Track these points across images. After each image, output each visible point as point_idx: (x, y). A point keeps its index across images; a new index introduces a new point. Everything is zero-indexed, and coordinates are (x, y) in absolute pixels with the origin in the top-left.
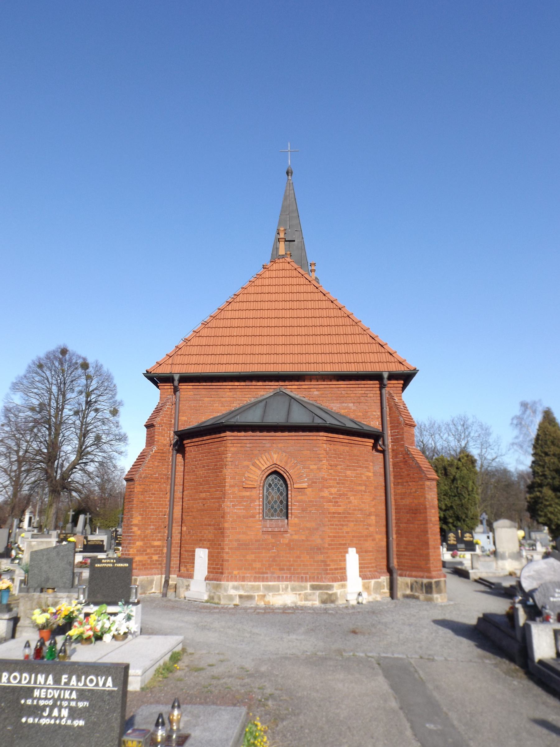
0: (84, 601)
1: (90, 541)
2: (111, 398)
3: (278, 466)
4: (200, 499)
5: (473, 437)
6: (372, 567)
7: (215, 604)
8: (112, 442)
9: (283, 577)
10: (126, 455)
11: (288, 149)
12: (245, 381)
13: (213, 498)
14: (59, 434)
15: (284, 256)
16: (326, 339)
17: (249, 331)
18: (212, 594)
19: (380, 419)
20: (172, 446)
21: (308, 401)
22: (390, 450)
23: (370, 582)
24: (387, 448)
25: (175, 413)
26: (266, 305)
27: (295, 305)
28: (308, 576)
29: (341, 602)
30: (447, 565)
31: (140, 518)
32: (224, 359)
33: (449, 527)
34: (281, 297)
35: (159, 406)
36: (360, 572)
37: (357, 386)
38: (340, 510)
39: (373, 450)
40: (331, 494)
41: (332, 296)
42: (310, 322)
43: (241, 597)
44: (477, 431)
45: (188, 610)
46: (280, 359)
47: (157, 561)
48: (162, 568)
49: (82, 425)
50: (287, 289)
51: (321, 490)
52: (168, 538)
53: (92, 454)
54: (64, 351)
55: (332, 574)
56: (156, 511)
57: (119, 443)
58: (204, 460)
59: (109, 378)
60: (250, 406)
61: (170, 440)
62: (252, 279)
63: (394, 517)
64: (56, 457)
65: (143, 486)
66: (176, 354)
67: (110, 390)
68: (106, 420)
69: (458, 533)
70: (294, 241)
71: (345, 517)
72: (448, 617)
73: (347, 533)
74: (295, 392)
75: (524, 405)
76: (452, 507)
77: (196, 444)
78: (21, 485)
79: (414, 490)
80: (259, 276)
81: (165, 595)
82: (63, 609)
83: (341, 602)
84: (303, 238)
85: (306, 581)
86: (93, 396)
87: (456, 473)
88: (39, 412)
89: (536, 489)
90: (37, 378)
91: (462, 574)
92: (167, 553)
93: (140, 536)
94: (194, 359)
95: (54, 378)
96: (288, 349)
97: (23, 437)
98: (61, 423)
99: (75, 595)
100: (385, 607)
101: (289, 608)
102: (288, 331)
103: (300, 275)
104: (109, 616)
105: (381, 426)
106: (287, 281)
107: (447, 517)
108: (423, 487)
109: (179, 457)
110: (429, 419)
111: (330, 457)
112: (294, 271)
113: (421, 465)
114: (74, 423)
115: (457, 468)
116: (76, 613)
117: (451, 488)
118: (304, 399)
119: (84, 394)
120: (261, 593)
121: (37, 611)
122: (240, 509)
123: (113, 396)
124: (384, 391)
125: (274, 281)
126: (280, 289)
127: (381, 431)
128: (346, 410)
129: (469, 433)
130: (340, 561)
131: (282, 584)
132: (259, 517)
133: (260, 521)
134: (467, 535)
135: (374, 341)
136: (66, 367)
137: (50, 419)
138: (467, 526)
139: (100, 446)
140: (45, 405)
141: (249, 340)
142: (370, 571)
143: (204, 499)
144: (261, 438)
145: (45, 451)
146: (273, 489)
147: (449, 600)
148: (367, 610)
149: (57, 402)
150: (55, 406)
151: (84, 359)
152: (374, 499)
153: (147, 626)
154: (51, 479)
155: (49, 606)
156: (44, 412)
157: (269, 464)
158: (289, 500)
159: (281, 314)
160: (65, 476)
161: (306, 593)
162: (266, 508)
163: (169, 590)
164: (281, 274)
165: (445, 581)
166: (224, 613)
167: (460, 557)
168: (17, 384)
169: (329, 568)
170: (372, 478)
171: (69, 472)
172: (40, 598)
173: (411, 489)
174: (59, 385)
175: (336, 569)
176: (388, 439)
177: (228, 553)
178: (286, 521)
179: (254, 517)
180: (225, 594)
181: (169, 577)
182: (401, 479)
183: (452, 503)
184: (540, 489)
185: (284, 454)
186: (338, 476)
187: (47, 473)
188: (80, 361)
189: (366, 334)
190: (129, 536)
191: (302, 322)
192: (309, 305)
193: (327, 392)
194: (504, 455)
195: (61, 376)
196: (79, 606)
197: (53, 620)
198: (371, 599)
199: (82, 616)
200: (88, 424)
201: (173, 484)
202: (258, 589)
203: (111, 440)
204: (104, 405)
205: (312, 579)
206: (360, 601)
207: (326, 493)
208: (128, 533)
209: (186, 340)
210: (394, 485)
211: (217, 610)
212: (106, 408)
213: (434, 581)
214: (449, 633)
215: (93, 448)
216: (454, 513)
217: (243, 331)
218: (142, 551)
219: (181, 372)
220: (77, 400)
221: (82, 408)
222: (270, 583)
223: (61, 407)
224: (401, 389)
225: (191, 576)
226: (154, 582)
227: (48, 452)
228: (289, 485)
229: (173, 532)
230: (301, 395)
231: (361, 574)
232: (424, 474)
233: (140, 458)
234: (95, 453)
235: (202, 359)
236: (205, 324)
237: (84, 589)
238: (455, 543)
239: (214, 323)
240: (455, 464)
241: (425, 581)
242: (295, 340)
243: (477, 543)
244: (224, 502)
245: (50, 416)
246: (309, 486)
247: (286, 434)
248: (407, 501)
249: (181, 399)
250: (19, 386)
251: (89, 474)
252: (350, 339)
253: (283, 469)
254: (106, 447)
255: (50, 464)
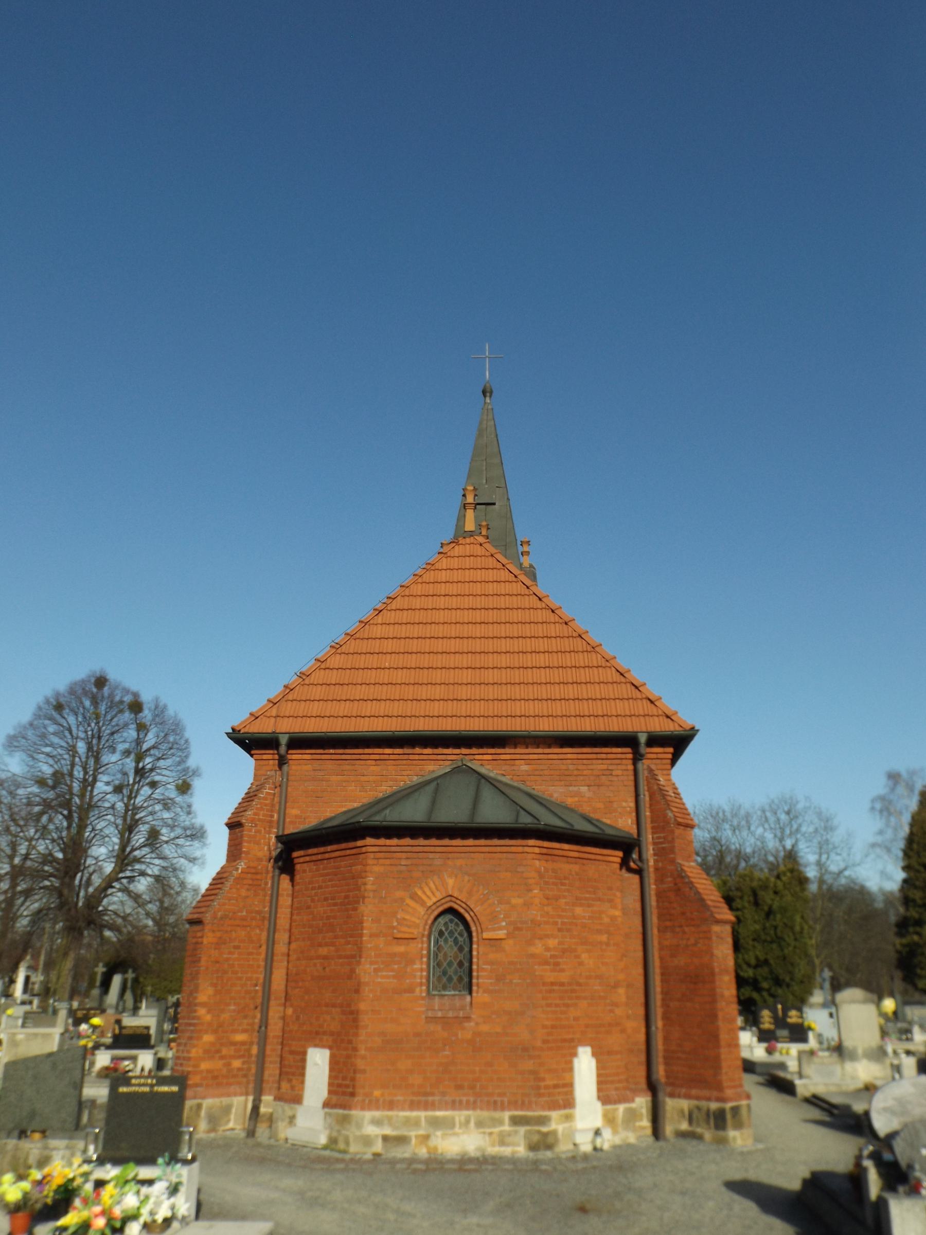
0: (95, 1157)
1: (125, 1028)
2: (179, 763)
3: (454, 899)
4: (318, 957)
5: (805, 833)
6: (620, 1081)
7: (340, 1152)
8: (180, 841)
9: (461, 1102)
10: (203, 863)
11: (485, 354)
12: (401, 747)
13: (340, 957)
14: (86, 826)
15: (473, 534)
16: (542, 676)
17: (412, 661)
18: (335, 1134)
19: (634, 814)
20: (272, 861)
21: (509, 782)
22: (651, 870)
23: (617, 1109)
24: (645, 866)
25: (280, 803)
26: (441, 616)
27: (491, 616)
28: (506, 1100)
29: (563, 1148)
30: (758, 1069)
31: (210, 991)
32: (368, 708)
33: (762, 996)
34: (468, 602)
35: (252, 790)
36: (599, 1090)
37: (594, 756)
38: (564, 977)
39: (621, 869)
40: (548, 949)
41: (554, 602)
42: (517, 645)
43: (385, 1138)
44: (812, 823)
45: (289, 1165)
46: (463, 708)
47: (239, 1069)
48: (248, 1083)
49: (127, 810)
50: (478, 589)
51: (530, 943)
52: (260, 1027)
53: (143, 862)
54: (101, 682)
55: (550, 1095)
56: (240, 979)
57: (191, 843)
58: (327, 887)
59: (177, 728)
60: (409, 790)
61: (269, 849)
62: (419, 572)
63: (658, 989)
64: (79, 865)
65: (218, 934)
66: (284, 699)
67: (178, 749)
68: (169, 801)
69: (776, 1009)
70: (494, 504)
71: (573, 991)
72: (754, 1175)
73: (576, 1019)
74: (488, 767)
75: (894, 777)
76: (766, 962)
77: (314, 858)
78: (15, 919)
79: (692, 941)
80: (430, 567)
81: (251, 1133)
82: (55, 1174)
83: (563, 1148)
84: (508, 499)
85: (503, 1109)
86: (148, 760)
87: (773, 900)
88: (53, 788)
89: (911, 929)
90: (52, 728)
91: (783, 1086)
92: (257, 1056)
93: (210, 1024)
94: (315, 708)
95: (81, 728)
96: (478, 692)
97: (22, 831)
98: (91, 806)
99: (81, 1144)
100: (642, 1157)
101: (471, 1160)
102: (478, 661)
103: (499, 566)
104: (139, 1186)
105: (635, 826)
106: (479, 575)
107: (759, 978)
108: (707, 936)
109: (285, 880)
110: (729, 801)
111: (546, 883)
112: (490, 558)
113: (705, 897)
114: (113, 807)
115: (776, 893)
116: (79, 1181)
117: (764, 929)
118: (503, 779)
119: (132, 756)
120: (422, 1132)
121: (8, 1177)
122: (388, 977)
123: (182, 761)
124: (640, 765)
125: (457, 576)
126: (466, 588)
127: (635, 836)
128: (576, 799)
129: (800, 826)
130: (564, 1070)
131: (459, 1116)
132: (421, 991)
133: (423, 998)
134: (793, 1013)
135: (623, 680)
136: (103, 708)
137: (71, 799)
138: (793, 994)
139: (157, 848)
140: (63, 775)
141: (410, 676)
142: (617, 1089)
143: (325, 958)
144: (426, 849)
145: (60, 855)
146: (446, 941)
147: (757, 1140)
148: (609, 1163)
149: (85, 769)
150: (81, 776)
151: (136, 695)
152: (624, 955)
153: (212, 1199)
154: (67, 907)
155: (30, 1167)
156: (61, 788)
157: (439, 896)
158: (475, 960)
159: (467, 630)
160: (93, 902)
161: (501, 1132)
162: (433, 974)
163: (259, 1125)
164: (469, 562)
165: (749, 1106)
166: (354, 1170)
167: (781, 1053)
168: (17, 737)
169: (542, 1084)
170: (620, 920)
171: (101, 894)
172: (16, 1148)
173: (688, 939)
174: (90, 740)
175: (556, 1086)
176: (647, 850)
177: (364, 1057)
178: (468, 998)
179: (411, 990)
180: (358, 1133)
181: (260, 1101)
182: (670, 920)
183: (766, 954)
184: (918, 929)
185: (466, 878)
186: (560, 916)
187: (60, 895)
188: (128, 699)
189: (610, 667)
190: (190, 1025)
191: (503, 645)
192: (516, 616)
193: (541, 767)
194: (859, 865)
195: (93, 725)
196: (86, 1168)
197: (36, 1195)
198: (617, 1140)
199: (89, 1187)
200: (136, 809)
201: (273, 930)
202: (417, 1123)
203: (178, 838)
204: (166, 775)
205: (513, 1105)
206: (598, 1145)
207: (538, 948)
208: (189, 1018)
209: (302, 675)
210: (659, 931)
211: (341, 1166)
212: (171, 780)
213: (728, 1105)
214: (748, 1208)
215: (146, 850)
216: (771, 972)
217: (400, 660)
218: (212, 1052)
219: (291, 731)
220: (121, 767)
221: (128, 781)
222: (439, 1113)
223: (90, 779)
224: (669, 761)
225: (297, 1099)
226: (234, 1110)
227: (65, 859)
228: (474, 934)
229: (270, 1017)
230: (498, 772)
231: (601, 1094)
232: (709, 913)
233: (215, 882)
234: (148, 860)
235: (330, 708)
236: (336, 648)
237: (97, 1135)
238: (772, 1027)
239: (352, 646)
240: (772, 885)
241: (714, 1106)
242: (490, 676)
243: (810, 1028)
244: (359, 963)
245: (71, 794)
246: (509, 935)
247: (470, 842)
248: (681, 961)
249: (290, 778)
250: (18, 741)
251: (136, 897)
252: (583, 675)
253: (464, 906)
254: (168, 850)
255: (67, 880)
